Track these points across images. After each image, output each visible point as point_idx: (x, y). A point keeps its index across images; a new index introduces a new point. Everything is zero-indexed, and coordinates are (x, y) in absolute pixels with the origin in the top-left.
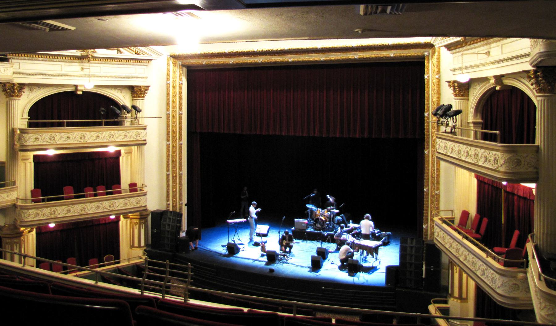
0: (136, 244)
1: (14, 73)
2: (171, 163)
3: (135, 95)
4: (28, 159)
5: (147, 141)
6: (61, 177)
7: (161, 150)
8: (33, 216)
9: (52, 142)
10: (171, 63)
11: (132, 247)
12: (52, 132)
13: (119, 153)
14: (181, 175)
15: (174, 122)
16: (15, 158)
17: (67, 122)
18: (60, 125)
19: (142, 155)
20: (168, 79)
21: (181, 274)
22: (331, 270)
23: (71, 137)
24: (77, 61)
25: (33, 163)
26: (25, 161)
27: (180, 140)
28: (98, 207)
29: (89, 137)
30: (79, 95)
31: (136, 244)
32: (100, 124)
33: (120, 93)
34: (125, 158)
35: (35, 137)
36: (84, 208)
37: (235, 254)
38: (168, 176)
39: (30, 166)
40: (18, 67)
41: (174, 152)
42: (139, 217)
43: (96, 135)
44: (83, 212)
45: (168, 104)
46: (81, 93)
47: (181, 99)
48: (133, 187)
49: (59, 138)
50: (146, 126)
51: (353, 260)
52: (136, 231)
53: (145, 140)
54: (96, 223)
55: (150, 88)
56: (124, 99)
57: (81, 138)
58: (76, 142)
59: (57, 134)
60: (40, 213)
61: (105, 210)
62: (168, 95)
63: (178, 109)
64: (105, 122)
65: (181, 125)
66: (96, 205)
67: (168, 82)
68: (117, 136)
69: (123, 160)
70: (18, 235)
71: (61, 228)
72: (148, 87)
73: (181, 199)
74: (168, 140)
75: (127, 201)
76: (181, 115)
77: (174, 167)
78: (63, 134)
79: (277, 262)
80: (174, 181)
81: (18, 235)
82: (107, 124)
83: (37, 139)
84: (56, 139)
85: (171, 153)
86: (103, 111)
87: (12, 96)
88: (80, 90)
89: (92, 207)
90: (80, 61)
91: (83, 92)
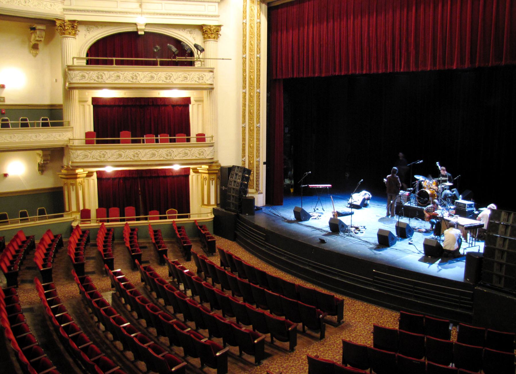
0: (206, 203)
1: (64, 9)
2: (247, 114)
3: (206, 36)
4: (86, 101)
5: (214, 86)
6: (117, 121)
8: (81, 157)
9: (100, 80)
11: (202, 204)
13: (187, 101)
14: (258, 128)
15: (251, 67)
17: (116, 60)
18: (111, 63)
19: (214, 103)
20: (245, 17)
22: (409, 253)
25: (92, 106)
26: (83, 104)
27: (259, 87)
28: (154, 155)
29: (142, 77)
30: (141, 35)
31: (206, 203)
32: (154, 64)
33: (189, 35)
34: (195, 107)
35: (81, 74)
36: (137, 154)
37: (301, 221)
38: (244, 128)
39: (90, 109)
41: (251, 101)
42: (207, 172)
43: (150, 75)
44: (136, 159)
45: (244, 47)
46: (143, 33)
47: (259, 41)
48: (201, 138)
49: (107, 76)
50: (214, 68)
51: (246, 197)
52: (206, 187)
53: (211, 84)
54: (162, 175)
55: (222, 28)
56: (190, 39)
57: (133, 78)
58: (127, 82)
59: (105, 72)
60: (89, 154)
61: (162, 159)
62: (244, 36)
63: (256, 52)
64: (160, 61)
65: (259, 70)
66: (151, 152)
67: (244, 21)
68: (175, 78)
69: (192, 109)
71: (123, 176)
72: (220, 26)
73: (258, 156)
74: (244, 87)
75: (187, 151)
76: (259, 59)
77: (251, 119)
79: (341, 234)
80: (251, 136)
83: (83, 76)
84: (104, 78)
85: (247, 103)
86: (156, 48)
87: (64, 34)
88: (141, 30)
89: (146, 154)
91: (145, 32)
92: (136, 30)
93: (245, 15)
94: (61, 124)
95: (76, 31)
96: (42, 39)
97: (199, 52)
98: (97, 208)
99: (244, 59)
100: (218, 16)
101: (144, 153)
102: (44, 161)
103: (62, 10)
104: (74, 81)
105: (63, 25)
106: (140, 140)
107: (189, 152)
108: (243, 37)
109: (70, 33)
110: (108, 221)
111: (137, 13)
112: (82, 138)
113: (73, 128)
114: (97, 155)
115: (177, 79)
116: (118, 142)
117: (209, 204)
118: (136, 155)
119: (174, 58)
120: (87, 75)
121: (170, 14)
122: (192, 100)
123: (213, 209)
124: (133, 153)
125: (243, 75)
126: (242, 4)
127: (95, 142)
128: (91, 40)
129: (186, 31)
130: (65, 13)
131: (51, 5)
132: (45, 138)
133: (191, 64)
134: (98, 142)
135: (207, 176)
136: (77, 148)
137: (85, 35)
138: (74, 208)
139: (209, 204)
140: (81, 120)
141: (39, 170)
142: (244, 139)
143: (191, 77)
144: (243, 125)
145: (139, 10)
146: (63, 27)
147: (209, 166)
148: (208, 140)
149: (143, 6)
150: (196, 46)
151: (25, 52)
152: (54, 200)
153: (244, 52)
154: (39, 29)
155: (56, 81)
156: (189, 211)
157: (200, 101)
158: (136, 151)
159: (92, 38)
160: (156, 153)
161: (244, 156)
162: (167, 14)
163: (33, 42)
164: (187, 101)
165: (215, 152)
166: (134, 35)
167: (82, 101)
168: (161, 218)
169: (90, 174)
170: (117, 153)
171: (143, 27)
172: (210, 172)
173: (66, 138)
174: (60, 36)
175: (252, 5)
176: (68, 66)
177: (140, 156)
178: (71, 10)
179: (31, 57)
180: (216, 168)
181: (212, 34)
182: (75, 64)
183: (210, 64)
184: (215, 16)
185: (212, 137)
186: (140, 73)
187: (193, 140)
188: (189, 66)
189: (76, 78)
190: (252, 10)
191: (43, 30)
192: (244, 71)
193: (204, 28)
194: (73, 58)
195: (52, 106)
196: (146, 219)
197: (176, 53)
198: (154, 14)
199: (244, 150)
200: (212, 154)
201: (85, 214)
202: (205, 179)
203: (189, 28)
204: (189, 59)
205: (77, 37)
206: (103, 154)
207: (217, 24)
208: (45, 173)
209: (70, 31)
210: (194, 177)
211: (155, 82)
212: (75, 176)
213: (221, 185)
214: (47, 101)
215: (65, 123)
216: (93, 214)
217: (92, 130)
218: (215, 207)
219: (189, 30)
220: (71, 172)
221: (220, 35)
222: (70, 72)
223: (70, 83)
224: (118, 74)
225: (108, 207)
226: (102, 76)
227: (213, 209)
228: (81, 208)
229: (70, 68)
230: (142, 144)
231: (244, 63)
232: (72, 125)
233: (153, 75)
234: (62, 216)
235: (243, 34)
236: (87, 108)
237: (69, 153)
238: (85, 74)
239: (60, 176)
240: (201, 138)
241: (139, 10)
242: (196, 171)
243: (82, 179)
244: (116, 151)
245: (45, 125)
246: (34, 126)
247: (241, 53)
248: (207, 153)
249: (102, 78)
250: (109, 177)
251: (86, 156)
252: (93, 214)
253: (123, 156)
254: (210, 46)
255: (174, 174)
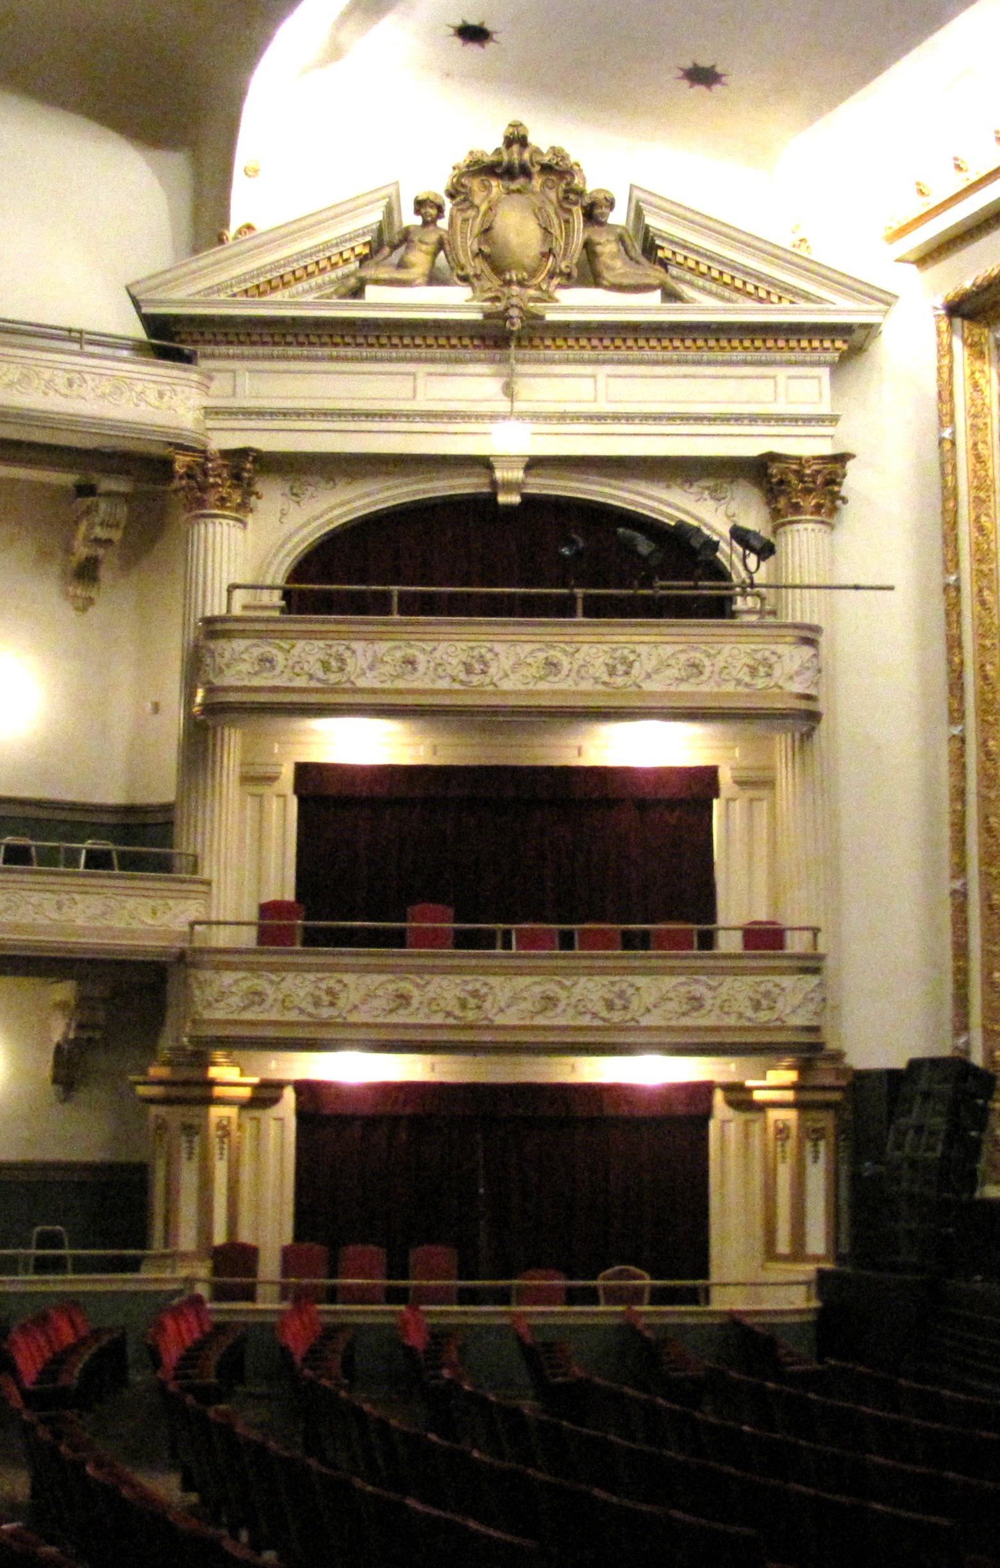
0: (783, 1246)
1: (211, 412)
3: (782, 503)
4: (271, 779)
5: (821, 707)
7: (929, 781)
9: (333, 678)
10: (957, 343)
12: (339, 636)
16: (205, 759)
17: (402, 595)
18: (378, 605)
19: (820, 789)
20: (946, 417)
21: (385, 931)
23: (421, 658)
24: (482, 354)
25: (293, 803)
28: (550, 1001)
29: (507, 664)
30: (509, 507)
31: (783, 1246)
32: (562, 608)
33: (711, 504)
35: (256, 652)
38: (960, 899)
39: (283, 813)
40: (229, 390)
43: (541, 656)
46: (515, 499)
50: (816, 629)
55: (850, 465)
56: (711, 514)
58: (443, 684)
59: (355, 645)
66: (538, 989)
67: (947, 433)
68: (649, 666)
70: (197, 1092)
72: (841, 459)
74: (956, 715)
78: (382, 647)
81: (197, 1092)
82: (598, 609)
83: (266, 662)
86: (570, 542)
87: (201, 503)
88: (510, 486)
89: (515, 999)
90: (497, 354)
92: (486, 490)
93: (946, 408)
94: (164, 866)
95: (251, 494)
96: (116, 535)
97: (752, 560)
98: (288, 1238)
99: (952, 591)
100: (833, 419)
101: (508, 993)
102: (81, 1026)
103: (200, 415)
104: (229, 679)
105: (198, 471)
106: (492, 934)
107: (708, 994)
108: (945, 500)
109: (223, 500)
110: (332, 1295)
111: (493, 417)
112: (246, 918)
113: (208, 883)
114: (302, 994)
115: (657, 671)
116: (397, 939)
117: (798, 1254)
118: (472, 1002)
119: (647, 583)
120: (280, 658)
121: (629, 418)
122: (725, 777)
123: (820, 1272)
124: (457, 992)
125: (950, 662)
126: (935, 364)
127: (299, 935)
128: (306, 531)
129: (694, 489)
130: (210, 424)
131: (161, 395)
132: (94, 918)
133: (719, 608)
134: (313, 939)
135: (790, 1116)
136: (226, 959)
137: (283, 514)
138: (187, 1240)
139: (798, 1254)
140: (249, 853)
141: (55, 1080)
142: (961, 950)
143: (720, 661)
144: (956, 731)
145: (503, 406)
146: (200, 478)
147: (804, 1068)
148: (796, 943)
149: (516, 388)
150: (740, 535)
151: (47, 593)
152: (111, 1204)
153: (951, 562)
154: (109, 494)
155: (156, 708)
156: (702, 1270)
157: (757, 782)
158: (475, 983)
159: (307, 523)
160: (563, 994)
161: (960, 870)
162: (616, 418)
163: (82, 551)
164: (701, 784)
165: (824, 1003)
166: (481, 507)
167: (256, 779)
168: (573, 1297)
169: (266, 1093)
170: (391, 987)
171: (518, 475)
172: (804, 1101)
173: (180, 925)
174: (186, 515)
175: (978, 365)
176: (209, 621)
177: (487, 1005)
178: (232, 413)
179: (66, 612)
180: (829, 1080)
181: (807, 491)
182: (237, 611)
183: (802, 608)
184: (820, 420)
185: (815, 931)
186: (498, 647)
187: (729, 942)
188: (710, 615)
189: (240, 667)
190: (976, 386)
191: (125, 496)
192: (954, 644)
193: (773, 470)
194: (232, 588)
195: (129, 810)
196: (503, 1297)
197: (654, 562)
198: (563, 417)
199: (961, 1000)
200: (812, 1007)
201: (234, 1261)
202: (782, 1132)
203: (709, 475)
204: (708, 589)
205: (250, 519)
206: (330, 992)
207: (826, 448)
208: (82, 1095)
209: (224, 492)
210: (733, 1129)
211: (563, 687)
212: (201, 1093)
213: (856, 1160)
214: (111, 791)
215: (177, 862)
216: (269, 1266)
217: (290, 896)
218: (828, 1266)
219: (710, 483)
220: (186, 1073)
221: (845, 500)
222: (212, 645)
223: (211, 690)
224: (410, 651)
225: (335, 1245)
226: (342, 661)
227: (820, 1272)
228: (220, 1238)
229: (214, 629)
230: (499, 951)
231: (953, 610)
232: (208, 871)
233: (556, 654)
234: (133, 1265)
235: (944, 487)
236: (275, 805)
237: (187, 986)
238: (275, 651)
239: (142, 1090)
240: (764, 938)
241: (503, 406)
242: (741, 1096)
243: (231, 1112)
244: (384, 977)
245: (98, 861)
246: (56, 864)
247: (938, 568)
248: (791, 1002)
249: (341, 670)
250: (349, 1110)
251: (256, 997)
252: (269, 1266)
253: (415, 1002)
254: (802, 541)
255: (640, 1113)
